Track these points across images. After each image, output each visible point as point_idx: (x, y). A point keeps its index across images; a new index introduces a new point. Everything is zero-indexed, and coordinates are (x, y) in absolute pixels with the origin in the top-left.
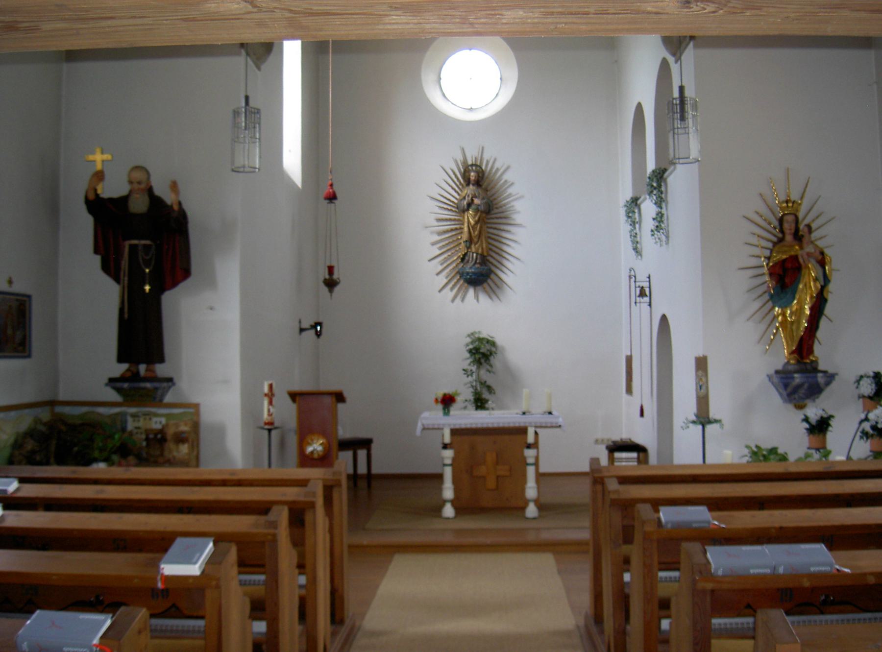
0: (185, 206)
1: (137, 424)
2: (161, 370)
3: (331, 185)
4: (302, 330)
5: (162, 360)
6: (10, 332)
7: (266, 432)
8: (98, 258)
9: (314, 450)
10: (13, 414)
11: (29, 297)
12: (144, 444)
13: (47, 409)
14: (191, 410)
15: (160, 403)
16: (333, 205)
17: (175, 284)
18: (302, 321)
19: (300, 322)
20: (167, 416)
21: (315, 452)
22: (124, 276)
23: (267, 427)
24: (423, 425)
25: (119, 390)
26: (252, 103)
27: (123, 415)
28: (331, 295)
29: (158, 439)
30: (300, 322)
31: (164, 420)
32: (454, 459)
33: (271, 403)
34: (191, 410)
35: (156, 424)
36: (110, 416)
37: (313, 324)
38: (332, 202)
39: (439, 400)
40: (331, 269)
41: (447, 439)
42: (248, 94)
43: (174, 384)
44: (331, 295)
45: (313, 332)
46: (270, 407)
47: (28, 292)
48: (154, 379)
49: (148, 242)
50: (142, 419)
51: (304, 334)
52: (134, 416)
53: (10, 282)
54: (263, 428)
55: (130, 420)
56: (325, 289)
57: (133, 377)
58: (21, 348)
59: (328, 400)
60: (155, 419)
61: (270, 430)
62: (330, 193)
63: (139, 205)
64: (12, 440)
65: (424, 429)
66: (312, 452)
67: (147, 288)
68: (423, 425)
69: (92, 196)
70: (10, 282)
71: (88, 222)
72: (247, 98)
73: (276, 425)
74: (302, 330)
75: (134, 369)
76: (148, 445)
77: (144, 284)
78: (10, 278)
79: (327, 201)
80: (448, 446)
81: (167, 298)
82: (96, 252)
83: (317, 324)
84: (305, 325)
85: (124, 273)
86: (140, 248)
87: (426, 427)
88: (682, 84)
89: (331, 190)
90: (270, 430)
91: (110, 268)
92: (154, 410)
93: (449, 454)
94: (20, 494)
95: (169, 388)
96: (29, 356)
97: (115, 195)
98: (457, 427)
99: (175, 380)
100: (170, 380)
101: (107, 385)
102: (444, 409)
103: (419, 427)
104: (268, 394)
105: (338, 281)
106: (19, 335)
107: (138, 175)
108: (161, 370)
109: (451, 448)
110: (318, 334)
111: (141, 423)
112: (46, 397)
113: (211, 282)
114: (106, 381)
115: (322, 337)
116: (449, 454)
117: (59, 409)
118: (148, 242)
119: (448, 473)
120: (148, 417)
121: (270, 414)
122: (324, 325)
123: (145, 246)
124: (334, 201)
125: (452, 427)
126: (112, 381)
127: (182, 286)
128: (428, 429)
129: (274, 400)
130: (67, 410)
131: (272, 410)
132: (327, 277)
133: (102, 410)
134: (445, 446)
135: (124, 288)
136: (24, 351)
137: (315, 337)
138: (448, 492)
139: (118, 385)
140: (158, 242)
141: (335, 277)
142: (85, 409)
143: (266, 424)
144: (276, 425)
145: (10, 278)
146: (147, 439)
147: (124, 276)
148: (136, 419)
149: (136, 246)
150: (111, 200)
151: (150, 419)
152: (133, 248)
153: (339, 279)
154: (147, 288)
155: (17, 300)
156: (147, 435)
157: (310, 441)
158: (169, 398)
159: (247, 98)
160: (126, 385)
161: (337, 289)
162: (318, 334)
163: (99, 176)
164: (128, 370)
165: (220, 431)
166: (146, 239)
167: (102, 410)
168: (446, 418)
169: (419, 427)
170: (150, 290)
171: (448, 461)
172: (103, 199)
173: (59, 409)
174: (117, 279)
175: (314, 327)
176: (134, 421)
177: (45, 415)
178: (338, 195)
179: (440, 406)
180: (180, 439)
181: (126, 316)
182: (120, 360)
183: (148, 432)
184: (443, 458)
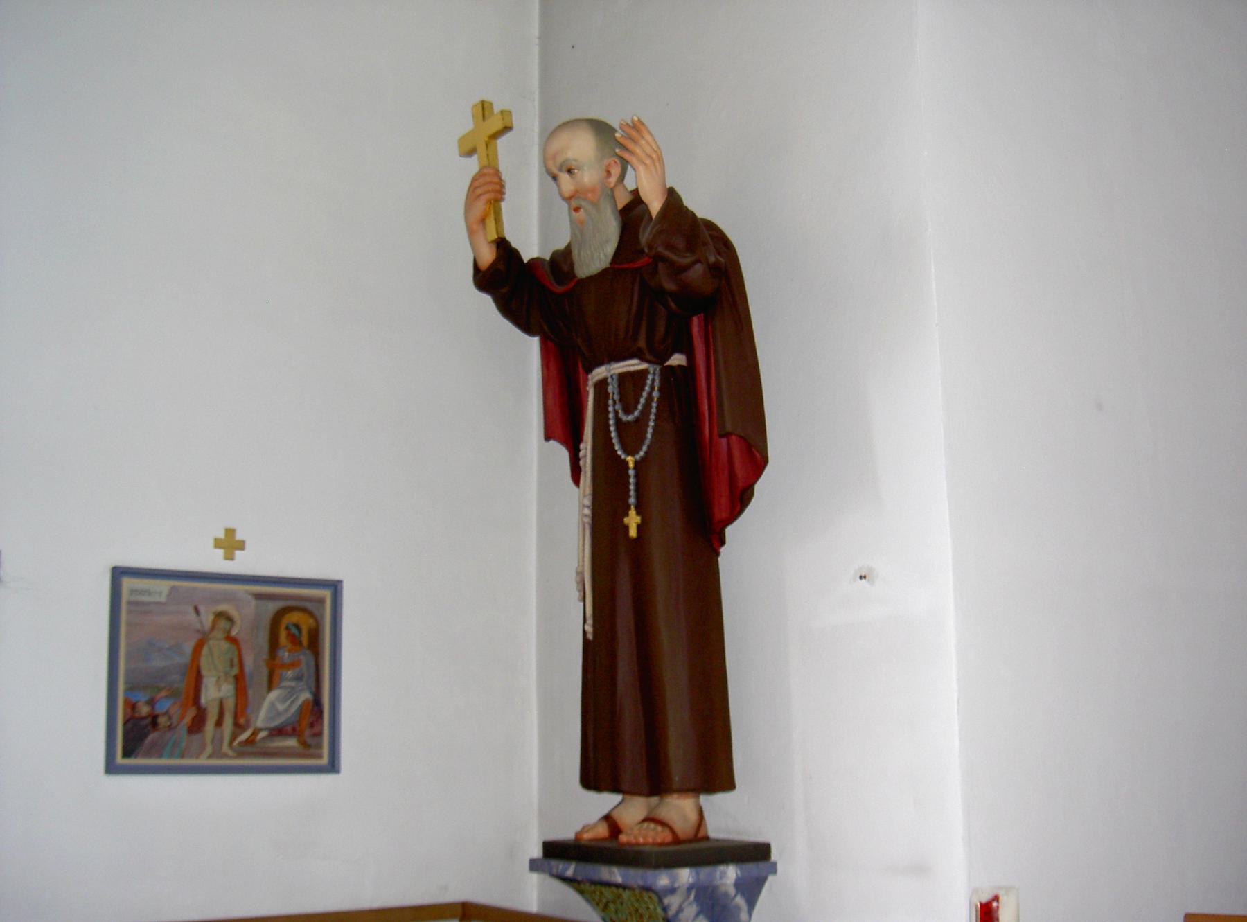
6: (215, 691)
11: (335, 587)
49: (633, 365)
101: (534, 865)
114: (536, 852)
123: (623, 377)
155: (259, 596)
182: (592, 778)
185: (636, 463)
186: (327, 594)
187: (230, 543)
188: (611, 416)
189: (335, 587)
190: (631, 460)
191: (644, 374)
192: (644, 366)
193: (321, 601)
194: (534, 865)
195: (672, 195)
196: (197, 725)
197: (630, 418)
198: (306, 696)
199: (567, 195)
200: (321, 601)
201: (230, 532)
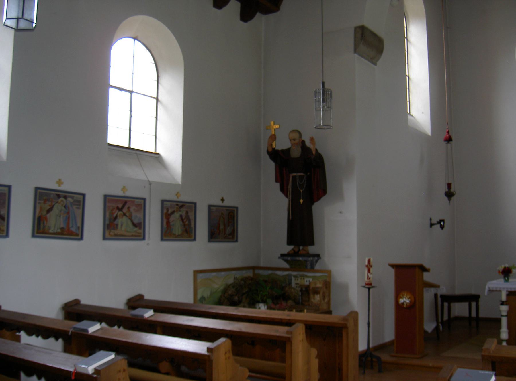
0: (320, 151)
1: (297, 282)
2: (311, 250)
3: (448, 132)
4: (432, 225)
5: (312, 243)
6: (222, 227)
7: (367, 289)
8: (278, 185)
9: (404, 302)
10: (223, 273)
11: (237, 208)
12: (300, 293)
13: (251, 271)
14: (326, 274)
15: (312, 268)
16: (449, 145)
17: (319, 199)
18: (432, 218)
19: (431, 219)
20: (314, 278)
21: (405, 303)
22: (289, 195)
23: (367, 286)
24: (489, 288)
25: (287, 261)
26: (326, 87)
27: (290, 275)
28: (450, 202)
29: (306, 291)
30: (431, 219)
31: (311, 279)
32: (509, 312)
33: (369, 271)
34: (326, 274)
35: (306, 282)
36: (283, 276)
37: (439, 221)
38: (449, 143)
39: (501, 271)
40: (449, 186)
41: (504, 298)
42: (324, 81)
43: (320, 258)
44: (450, 202)
45: (439, 225)
46: (369, 274)
47: (236, 205)
48: (309, 255)
49: (302, 174)
50: (299, 279)
51: (433, 227)
52: (296, 277)
53: (223, 200)
54: (364, 287)
55: (293, 279)
56: (224, 198)
57: (294, 254)
58: (231, 237)
59: (417, 270)
60: (306, 279)
61: (369, 289)
62: (447, 137)
63: (296, 153)
64: (222, 288)
65: (490, 291)
66: (403, 303)
67: (301, 201)
68: (489, 288)
69: (270, 150)
70: (223, 200)
71: (272, 165)
72: (323, 83)
73: (373, 285)
74: (432, 225)
75: (296, 250)
76: (302, 294)
77: (300, 199)
78: (223, 198)
79: (446, 142)
80: (504, 303)
81: (316, 207)
82: (277, 181)
83: (441, 221)
84: (434, 221)
85: (290, 193)
86: (297, 178)
87: (491, 289)
88: (134, 41)
89: (448, 135)
90: (369, 289)
91: (283, 189)
92: (306, 273)
93: (504, 309)
94: (153, 319)
95: (317, 261)
96: (237, 241)
97: (285, 148)
98: (513, 290)
99: (321, 256)
100: (318, 256)
101: (279, 258)
102: (504, 277)
103: (487, 289)
104: (367, 265)
105: (454, 193)
106: (229, 230)
107: (296, 135)
108: (311, 250)
109: (506, 304)
110: (442, 227)
111: (299, 281)
112: (251, 265)
113: (340, 196)
114: (279, 256)
115: (444, 229)
116: (504, 309)
117: (257, 271)
118: (302, 174)
119: (504, 321)
120: (302, 278)
121: (368, 278)
122: (446, 221)
123: (300, 176)
124: (451, 142)
125: (509, 290)
126: (283, 256)
127: (323, 199)
128: (493, 291)
129: (371, 270)
130: (261, 272)
131: (369, 276)
132: (447, 190)
133: (279, 273)
134: (503, 303)
135: (289, 201)
136: (233, 238)
137: (440, 229)
138: (504, 334)
139: (285, 258)
140: (309, 174)
141: (452, 190)
142: (270, 272)
143: (366, 284)
144: (373, 285)
145: (223, 198)
146: (301, 291)
147: (289, 195)
148: (297, 278)
149: (295, 176)
150: (282, 151)
151: (304, 279)
152: (294, 177)
153: (455, 191)
154: (301, 201)
155: (227, 210)
156: (302, 288)
157: (401, 296)
158: (317, 267)
159: (323, 83)
160: (289, 258)
161: (453, 198)
162: (442, 227)
163: (273, 138)
164: (293, 250)
165: (345, 288)
166: (299, 172)
167: (279, 273)
168: (506, 283)
169: (487, 289)
170: (303, 202)
171: (505, 313)
172: (278, 151)
173: (257, 271)
174: (286, 196)
175: (439, 222)
176: (295, 279)
177: (249, 274)
178: (453, 138)
179: (502, 276)
180: (316, 291)
181: (290, 218)
182: (289, 243)
183: (301, 286)
184: (500, 311)
185: (302, 191)
186: (235, 209)
187: (60, 182)
188: (297, 183)
189: (237, 208)
190: (301, 191)
191: (304, 176)
192: (304, 175)
193: (234, 210)
194: (279, 258)
195: (316, 150)
196: (219, 234)
197: (301, 183)
198: (233, 228)
199: (5, 24)
200: (234, 210)
201: (60, 180)
